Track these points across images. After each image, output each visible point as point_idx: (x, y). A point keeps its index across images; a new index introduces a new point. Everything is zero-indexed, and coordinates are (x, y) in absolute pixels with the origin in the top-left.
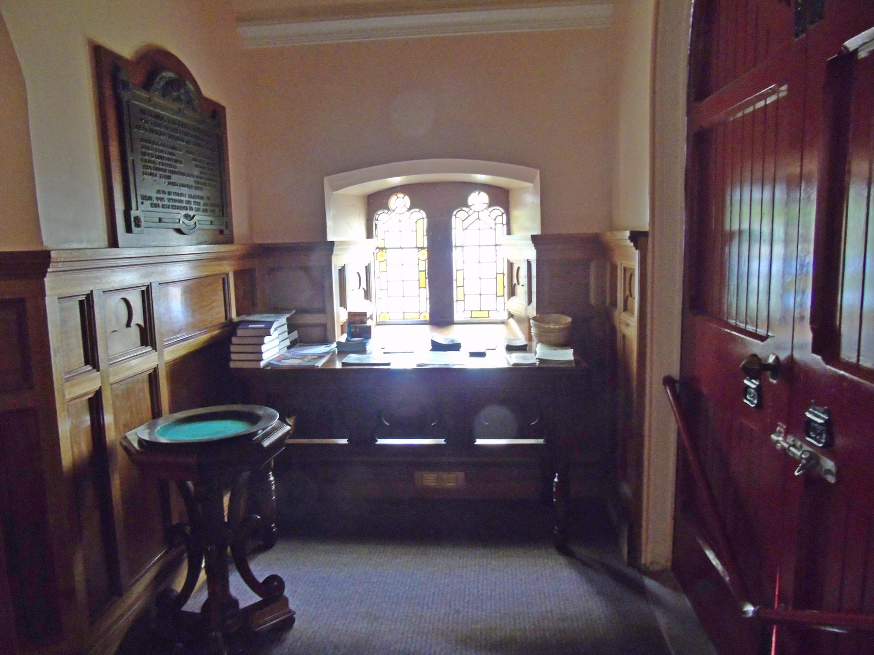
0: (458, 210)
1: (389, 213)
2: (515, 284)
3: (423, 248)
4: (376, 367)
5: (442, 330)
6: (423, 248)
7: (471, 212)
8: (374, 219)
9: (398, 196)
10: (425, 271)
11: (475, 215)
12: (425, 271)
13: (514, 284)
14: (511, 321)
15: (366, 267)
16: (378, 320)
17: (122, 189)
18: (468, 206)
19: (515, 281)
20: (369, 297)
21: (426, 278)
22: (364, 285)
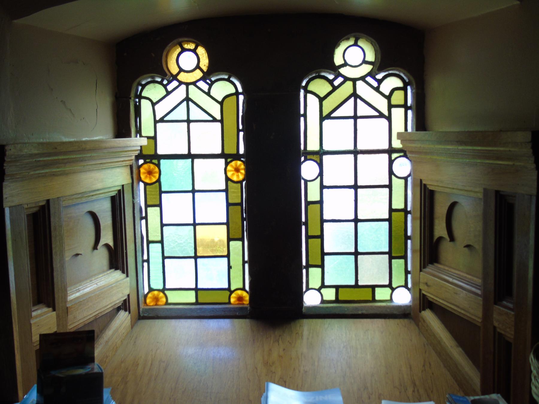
0: (310, 77)
1: (165, 82)
2: (440, 239)
3: (236, 157)
4: (241, 114)
5: (278, 332)
6: (236, 157)
7: (340, 80)
8: (132, 95)
9: (198, 71)
10: (241, 204)
11: (348, 87)
12: (241, 204)
13: (436, 238)
14: (428, 315)
15: (113, 199)
16: (142, 306)
17: (130, 115)
18: (335, 69)
19: (440, 230)
20: (120, 265)
21: (243, 219)
22: (107, 238)
